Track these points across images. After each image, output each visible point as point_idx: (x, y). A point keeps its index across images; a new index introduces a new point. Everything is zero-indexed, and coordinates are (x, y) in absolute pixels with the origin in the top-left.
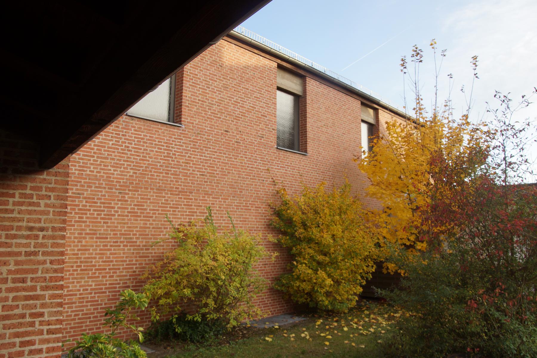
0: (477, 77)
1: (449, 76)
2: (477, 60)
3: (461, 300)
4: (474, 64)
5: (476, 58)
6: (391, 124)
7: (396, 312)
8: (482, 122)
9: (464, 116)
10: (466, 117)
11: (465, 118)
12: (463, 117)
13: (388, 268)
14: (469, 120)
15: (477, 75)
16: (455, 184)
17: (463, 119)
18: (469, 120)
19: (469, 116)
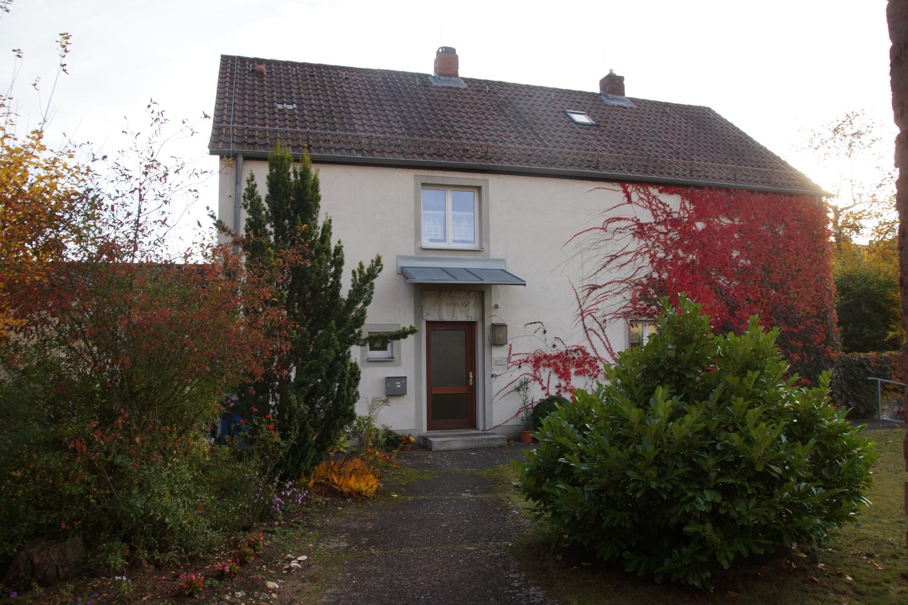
0: (65, 71)
1: (16, 53)
2: (69, 41)
3: (56, 444)
4: (63, 46)
5: (68, 38)
6: (639, 448)
7: (298, 309)
8: (67, 149)
9: (36, 132)
10: (39, 134)
11: (37, 137)
12: (33, 133)
13: (110, 550)
14: (43, 142)
15: (65, 68)
16: (110, 361)
17: (33, 138)
18: (43, 142)
19: (44, 134)
